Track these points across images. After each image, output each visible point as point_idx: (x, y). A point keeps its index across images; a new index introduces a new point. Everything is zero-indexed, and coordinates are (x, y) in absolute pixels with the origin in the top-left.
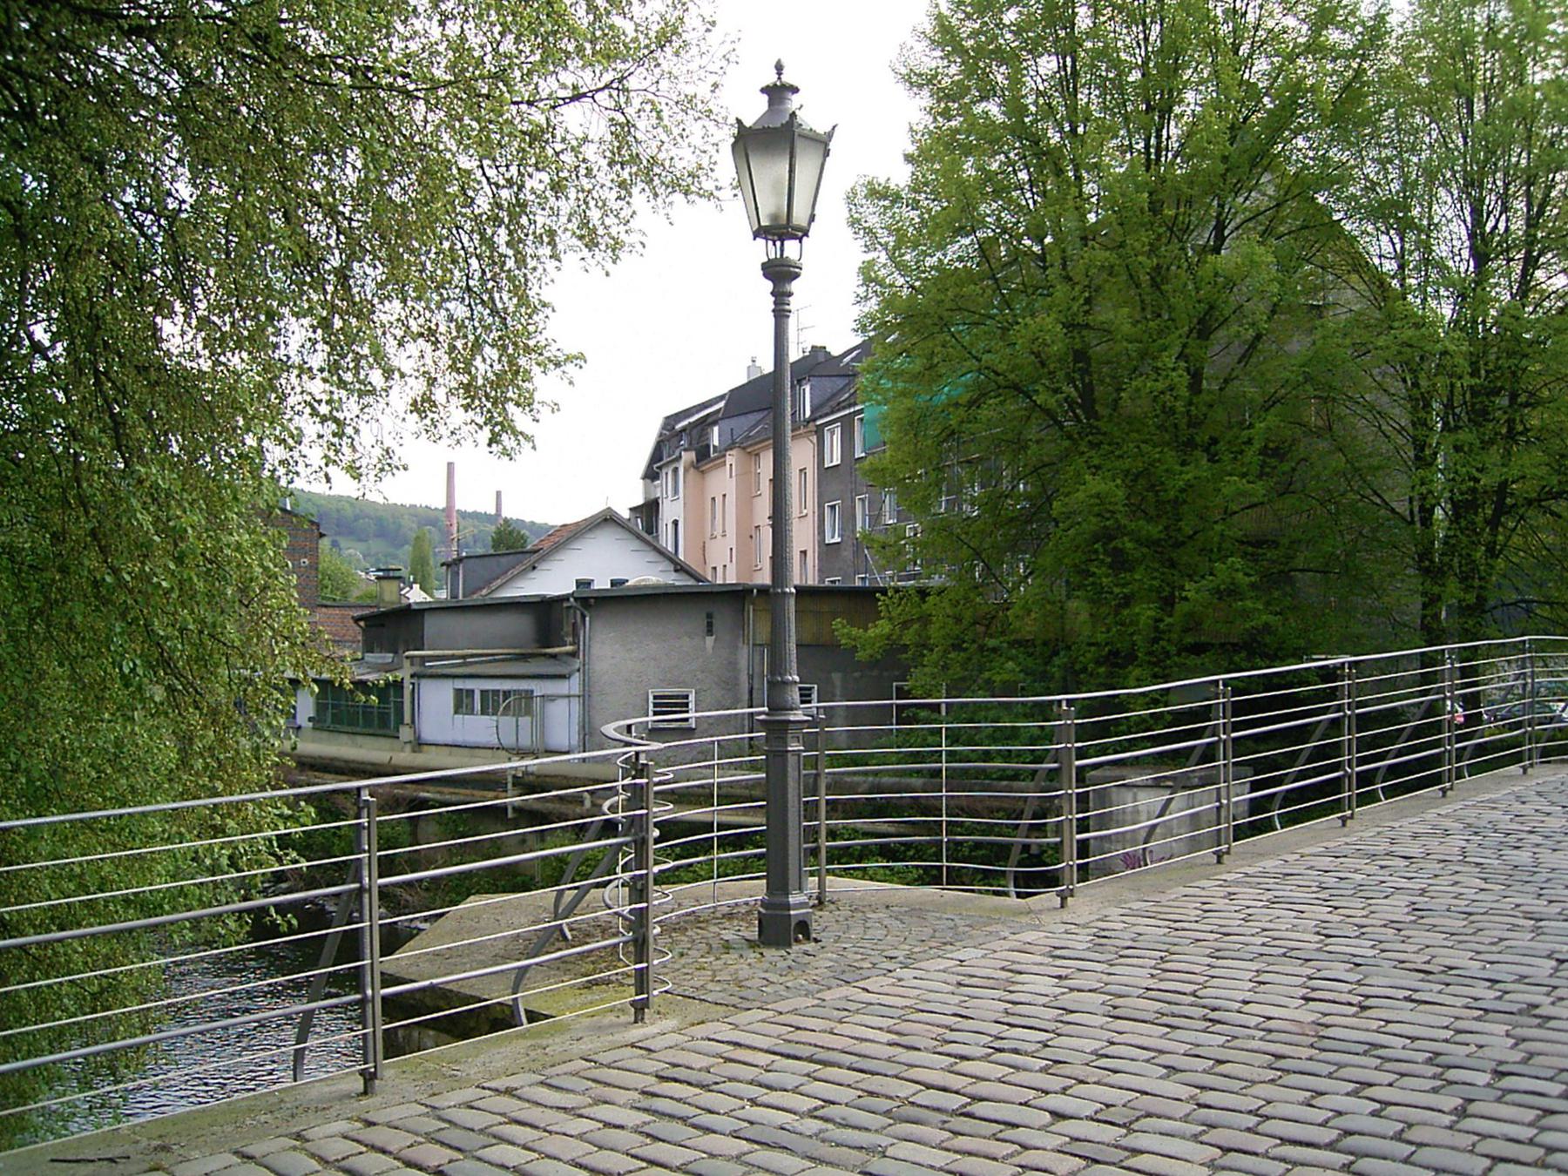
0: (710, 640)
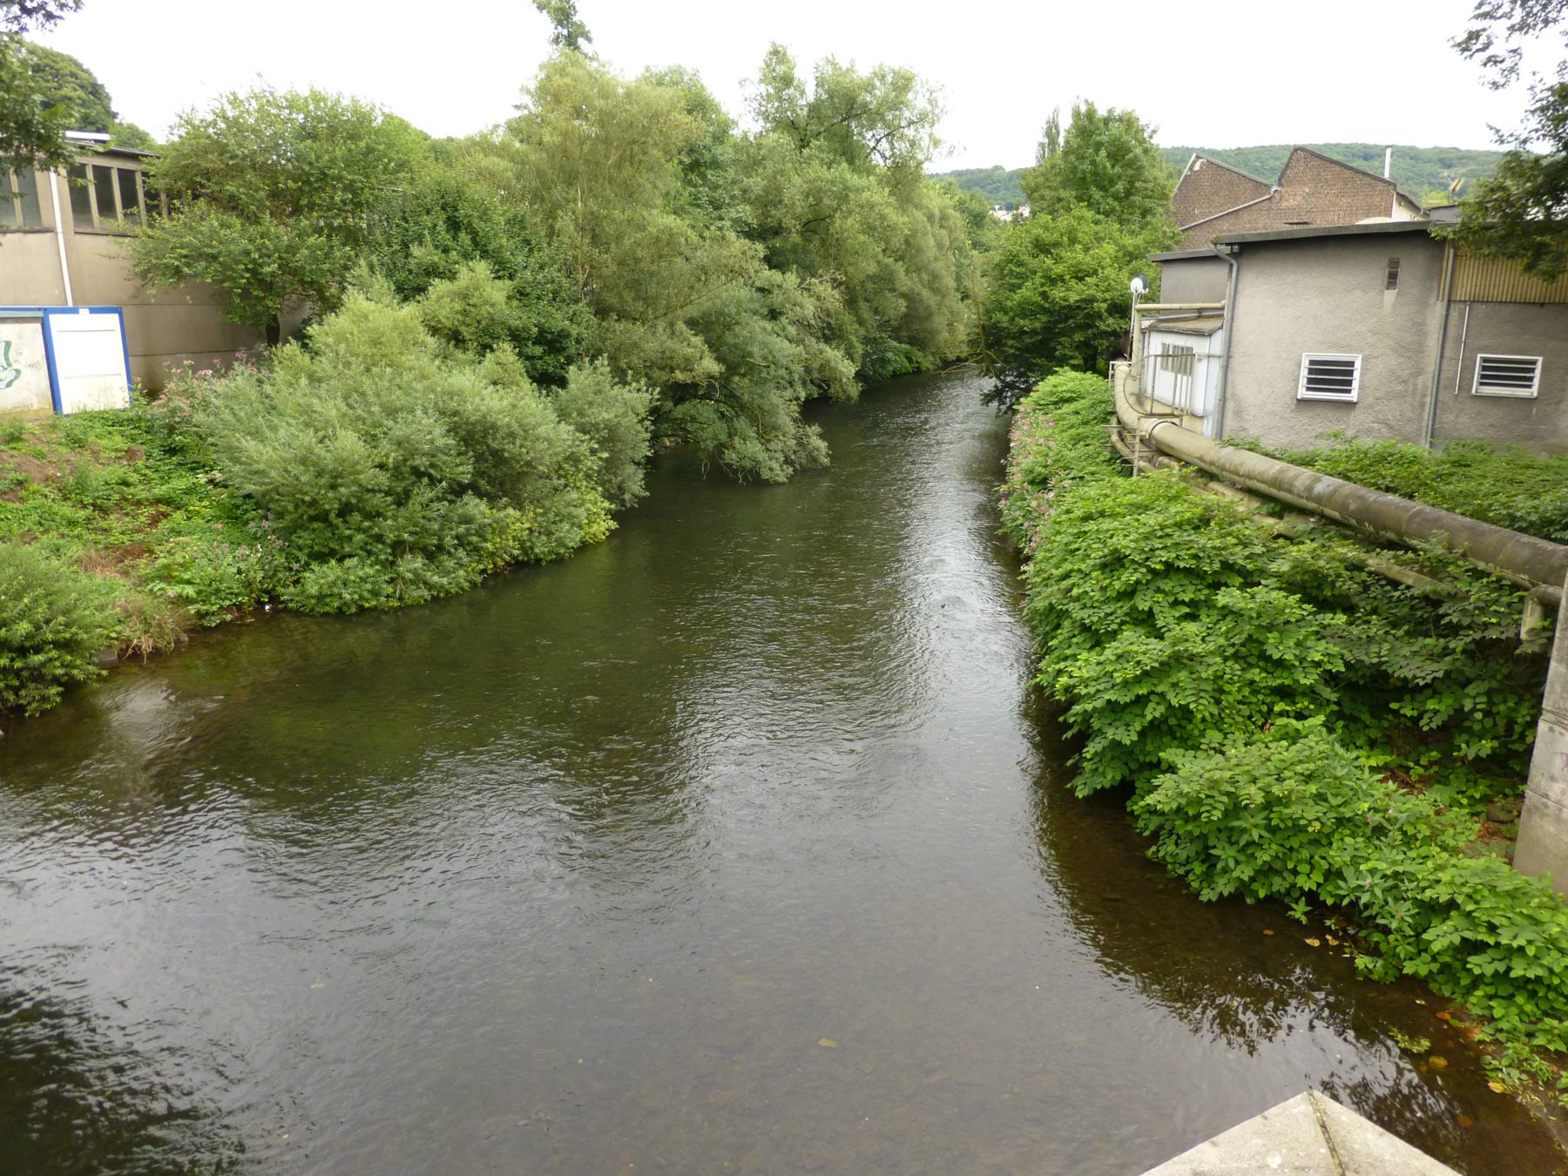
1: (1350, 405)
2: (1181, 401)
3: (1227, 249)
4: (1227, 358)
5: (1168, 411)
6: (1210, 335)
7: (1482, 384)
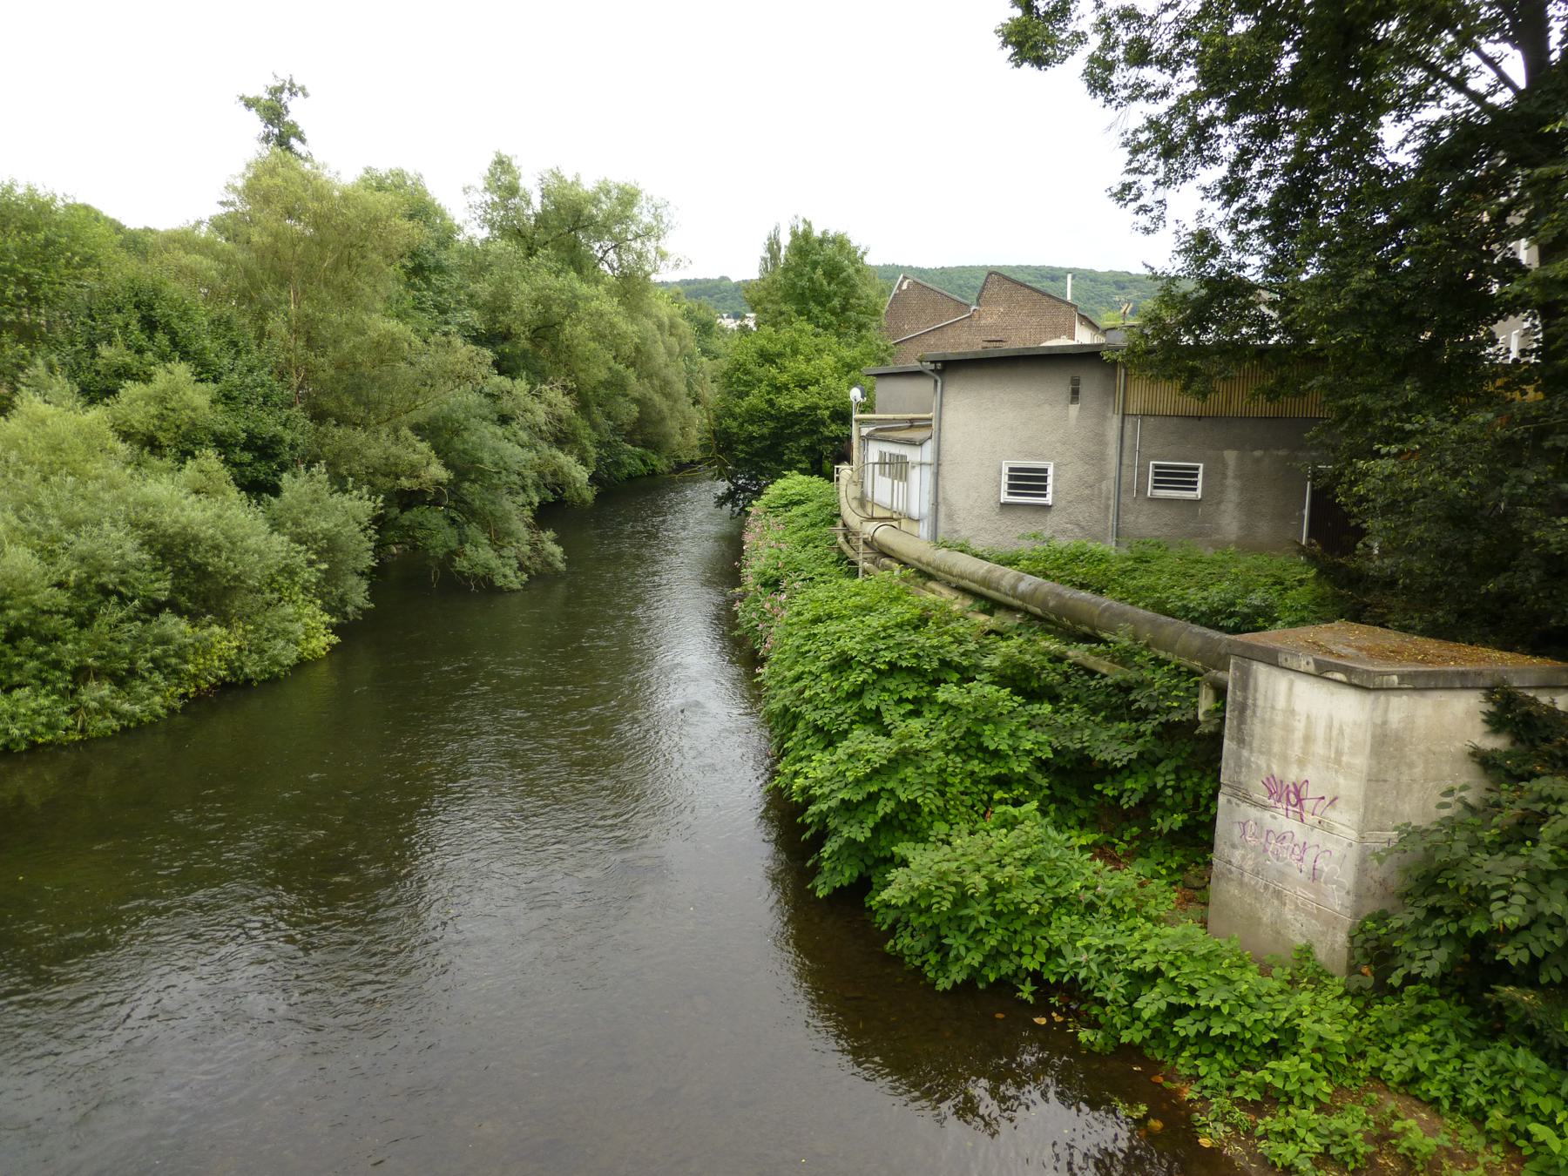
0: (1074, 409)
1: (1046, 508)
2: (899, 505)
3: (932, 366)
4: (937, 465)
5: (888, 514)
6: (921, 445)
7: (1155, 488)
